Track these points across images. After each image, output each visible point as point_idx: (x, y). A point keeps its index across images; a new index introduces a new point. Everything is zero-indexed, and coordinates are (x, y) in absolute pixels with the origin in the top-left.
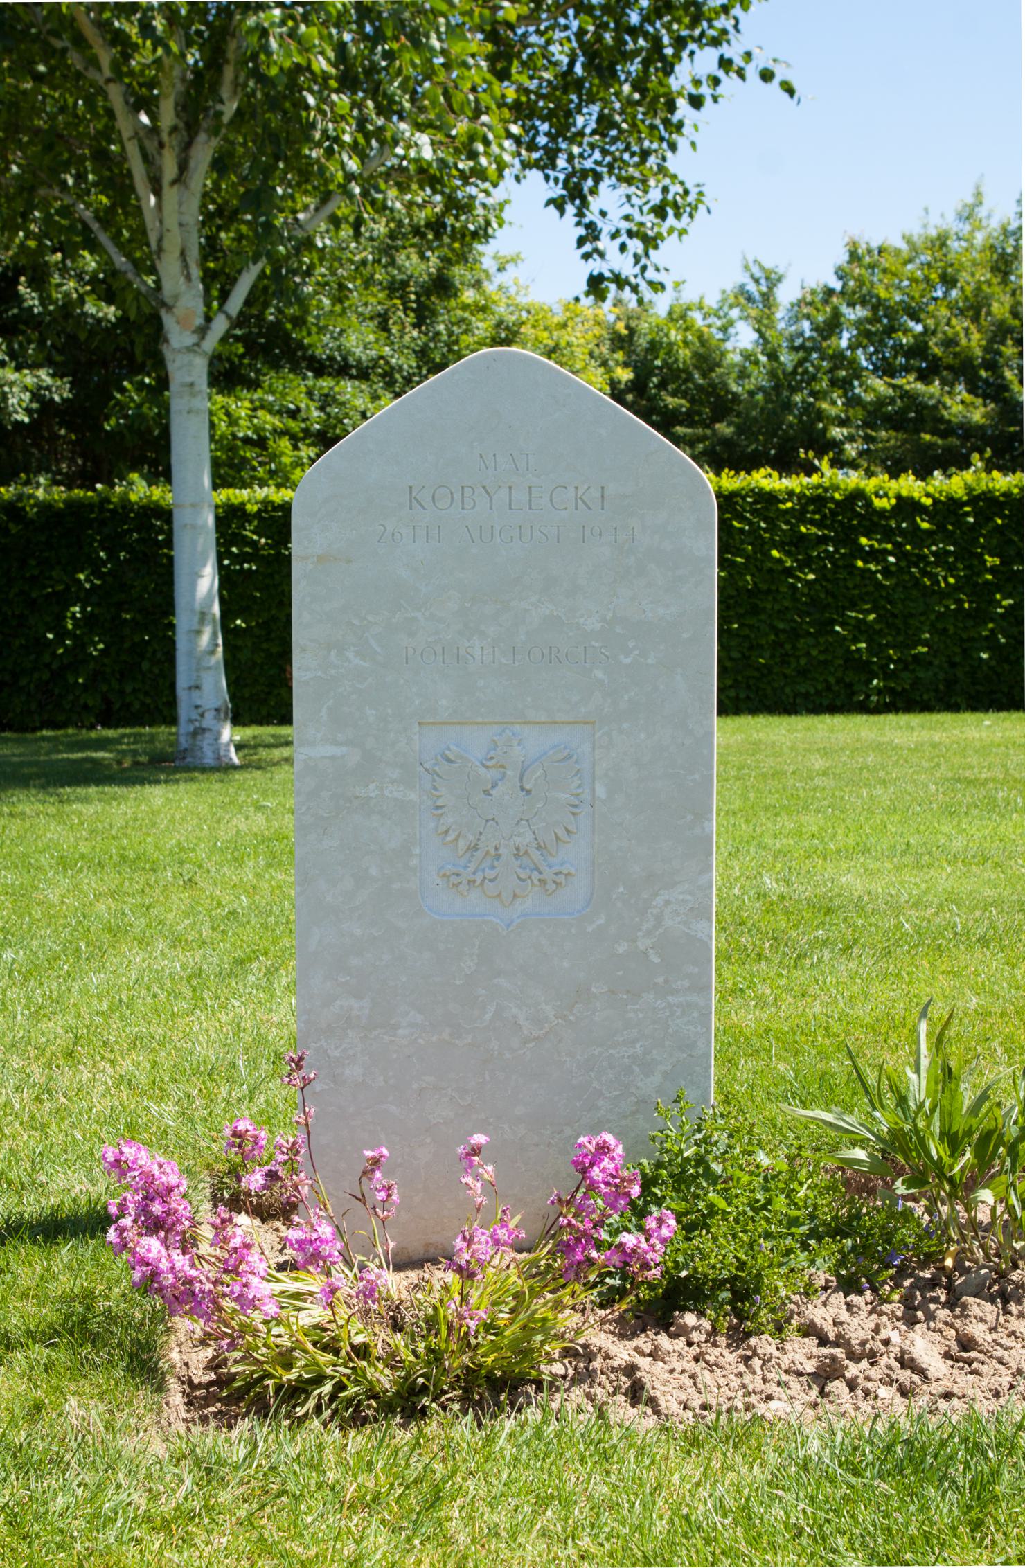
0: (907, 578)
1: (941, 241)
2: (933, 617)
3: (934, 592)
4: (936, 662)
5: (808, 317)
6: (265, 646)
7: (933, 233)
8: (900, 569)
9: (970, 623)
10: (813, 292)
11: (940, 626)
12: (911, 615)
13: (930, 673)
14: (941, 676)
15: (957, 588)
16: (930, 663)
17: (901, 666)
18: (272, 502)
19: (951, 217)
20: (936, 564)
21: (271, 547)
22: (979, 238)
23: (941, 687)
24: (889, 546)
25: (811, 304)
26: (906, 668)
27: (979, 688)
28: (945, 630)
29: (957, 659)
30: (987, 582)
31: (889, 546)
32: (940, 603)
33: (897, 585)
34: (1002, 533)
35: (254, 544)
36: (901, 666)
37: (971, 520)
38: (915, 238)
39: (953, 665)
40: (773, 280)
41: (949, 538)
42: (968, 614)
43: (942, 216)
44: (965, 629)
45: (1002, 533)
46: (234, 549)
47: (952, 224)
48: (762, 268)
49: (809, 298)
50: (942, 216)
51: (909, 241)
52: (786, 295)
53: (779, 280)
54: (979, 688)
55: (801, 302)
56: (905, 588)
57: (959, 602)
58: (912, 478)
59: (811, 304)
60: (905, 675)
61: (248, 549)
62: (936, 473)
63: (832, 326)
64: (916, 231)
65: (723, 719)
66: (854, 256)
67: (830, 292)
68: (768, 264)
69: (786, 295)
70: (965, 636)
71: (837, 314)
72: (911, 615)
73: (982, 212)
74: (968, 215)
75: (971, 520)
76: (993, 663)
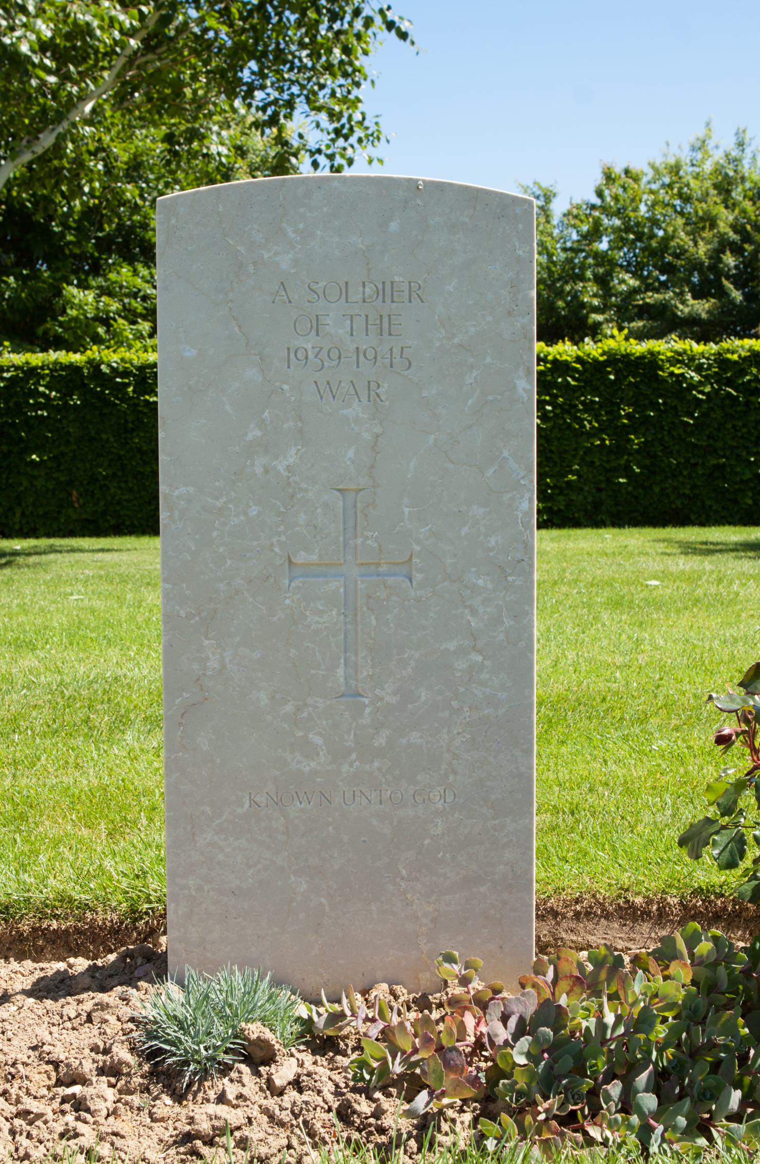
0: (561, 422)
1: (675, 169)
2: (581, 453)
3: (583, 433)
4: (586, 488)
5: (574, 226)
6: (55, 475)
7: (672, 161)
8: (556, 415)
9: (613, 457)
10: (578, 207)
11: (588, 459)
12: (566, 451)
13: (581, 497)
14: (590, 499)
15: (601, 430)
16: (582, 489)
17: (557, 491)
18: (61, 363)
19: (686, 148)
20: (585, 411)
21: (60, 399)
22: (708, 167)
23: (589, 508)
24: (548, 398)
25: (576, 217)
26: (561, 493)
27: (620, 508)
28: (592, 462)
29: (603, 486)
30: (624, 425)
31: (548, 398)
32: (587, 441)
33: (553, 428)
34: (637, 387)
35: (47, 397)
36: (557, 491)
37: (612, 377)
38: (657, 164)
39: (599, 490)
40: (548, 197)
41: (595, 391)
42: (610, 450)
43: (680, 147)
44: (608, 461)
45: (637, 387)
46: (31, 401)
47: (685, 156)
48: (540, 187)
49: (575, 212)
50: (680, 147)
51: (653, 166)
52: (558, 208)
53: (555, 195)
54: (620, 508)
55: (567, 214)
56: (560, 429)
57: (603, 440)
58: (568, 343)
59: (576, 217)
60: (561, 498)
61: (42, 400)
62: (587, 340)
63: (595, 233)
64: (659, 161)
65: (544, 532)
66: (609, 178)
67: (593, 207)
68: (544, 184)
69: (558, 208)
70: (608, 466)
71: (597, 223)
72: (566, 451)
73: (711, 144)
74: (701, 146)
75: (612, 377)
76: (630, 489)
